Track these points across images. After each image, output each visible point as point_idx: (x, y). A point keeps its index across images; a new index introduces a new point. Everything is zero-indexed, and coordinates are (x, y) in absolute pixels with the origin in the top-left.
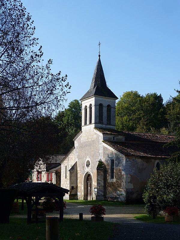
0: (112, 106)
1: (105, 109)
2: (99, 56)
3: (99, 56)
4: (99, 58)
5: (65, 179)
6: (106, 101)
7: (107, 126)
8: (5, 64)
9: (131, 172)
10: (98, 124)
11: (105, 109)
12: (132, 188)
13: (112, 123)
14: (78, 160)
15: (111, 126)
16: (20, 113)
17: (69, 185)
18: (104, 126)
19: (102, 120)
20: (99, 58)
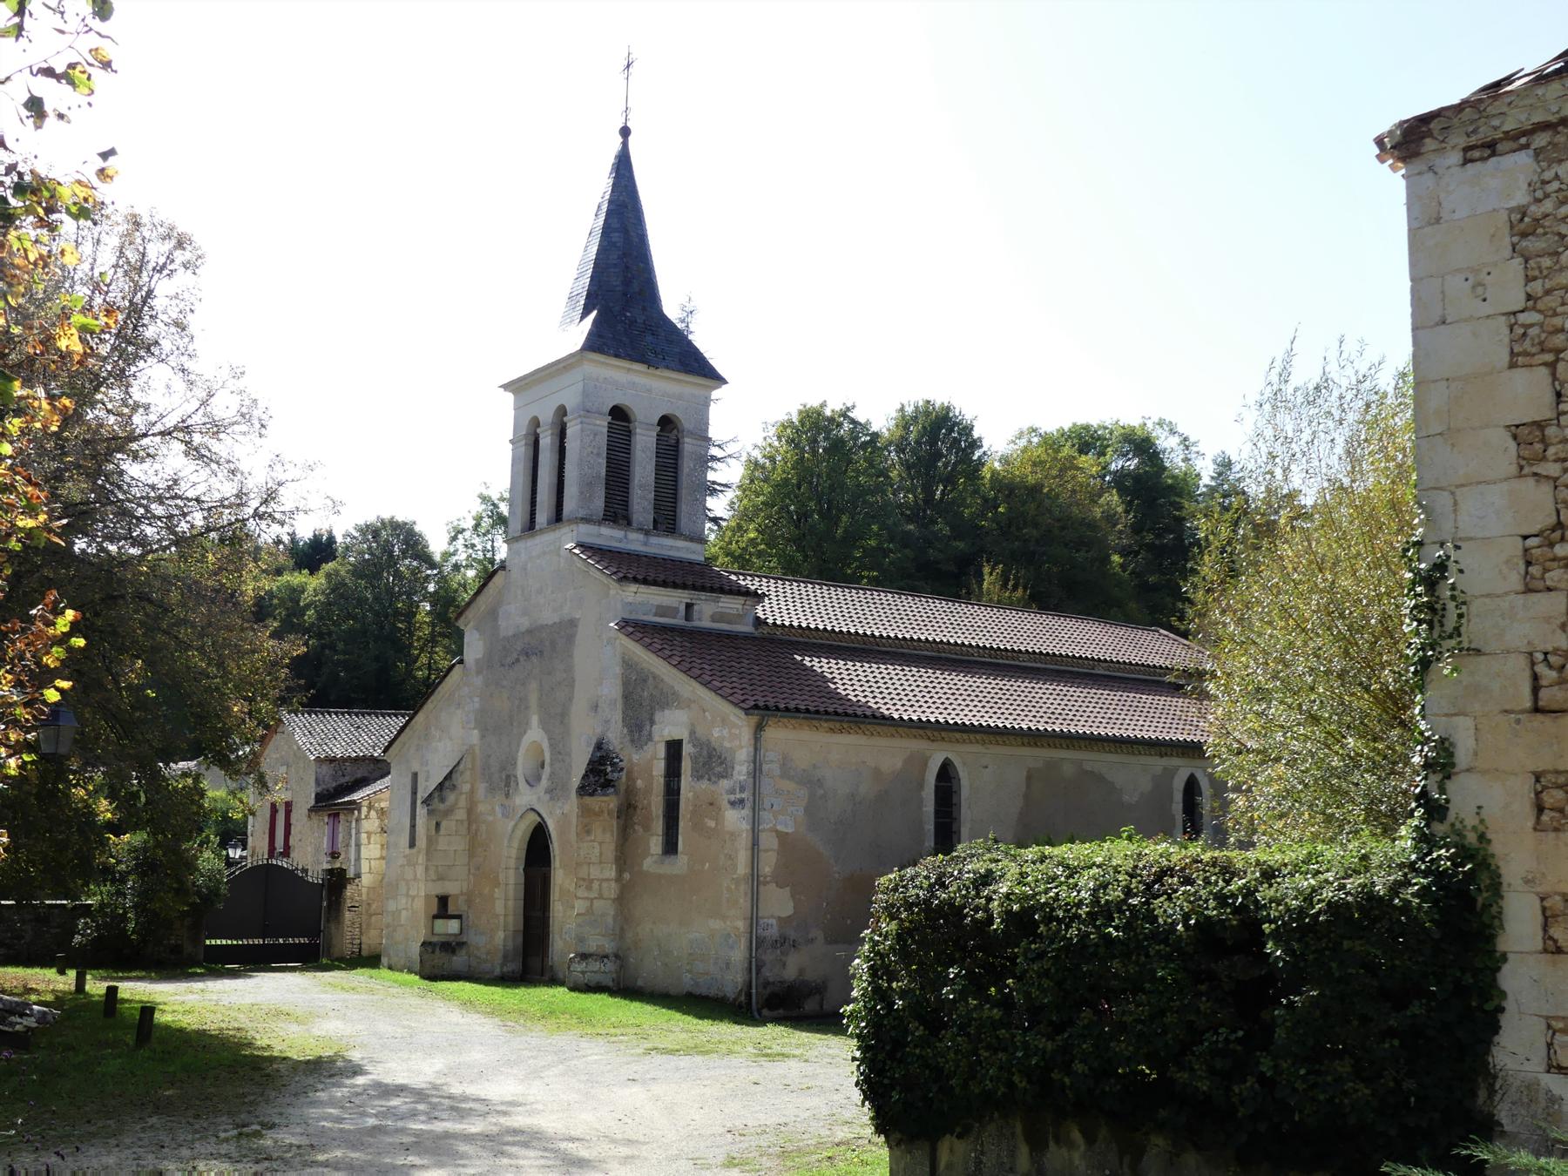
0: (687, 423)
1: (644, 443)
2: (625, 132)
3: (625, 132)
4: (625, 145)
5: (407, 851)
6: (648, 390)
7: (654, 540)
8: (1316, 780)
9: (781, 817)
10: (600, 523)
11: (644, 443)
12: (784, 915)
13: (684, 522)
14: (483, 737)
15: (680, 543)
16: (872, 505)
17: (619, 706)
18: (634, 541)
19: (626, 504)
20: (625, 145)
